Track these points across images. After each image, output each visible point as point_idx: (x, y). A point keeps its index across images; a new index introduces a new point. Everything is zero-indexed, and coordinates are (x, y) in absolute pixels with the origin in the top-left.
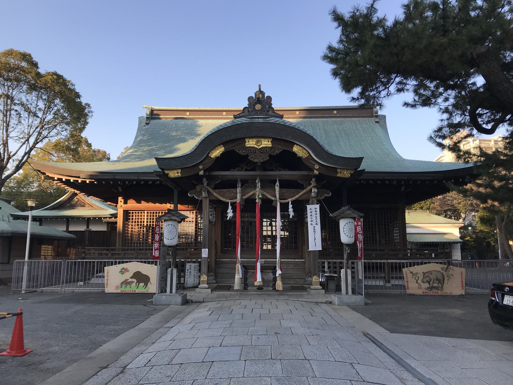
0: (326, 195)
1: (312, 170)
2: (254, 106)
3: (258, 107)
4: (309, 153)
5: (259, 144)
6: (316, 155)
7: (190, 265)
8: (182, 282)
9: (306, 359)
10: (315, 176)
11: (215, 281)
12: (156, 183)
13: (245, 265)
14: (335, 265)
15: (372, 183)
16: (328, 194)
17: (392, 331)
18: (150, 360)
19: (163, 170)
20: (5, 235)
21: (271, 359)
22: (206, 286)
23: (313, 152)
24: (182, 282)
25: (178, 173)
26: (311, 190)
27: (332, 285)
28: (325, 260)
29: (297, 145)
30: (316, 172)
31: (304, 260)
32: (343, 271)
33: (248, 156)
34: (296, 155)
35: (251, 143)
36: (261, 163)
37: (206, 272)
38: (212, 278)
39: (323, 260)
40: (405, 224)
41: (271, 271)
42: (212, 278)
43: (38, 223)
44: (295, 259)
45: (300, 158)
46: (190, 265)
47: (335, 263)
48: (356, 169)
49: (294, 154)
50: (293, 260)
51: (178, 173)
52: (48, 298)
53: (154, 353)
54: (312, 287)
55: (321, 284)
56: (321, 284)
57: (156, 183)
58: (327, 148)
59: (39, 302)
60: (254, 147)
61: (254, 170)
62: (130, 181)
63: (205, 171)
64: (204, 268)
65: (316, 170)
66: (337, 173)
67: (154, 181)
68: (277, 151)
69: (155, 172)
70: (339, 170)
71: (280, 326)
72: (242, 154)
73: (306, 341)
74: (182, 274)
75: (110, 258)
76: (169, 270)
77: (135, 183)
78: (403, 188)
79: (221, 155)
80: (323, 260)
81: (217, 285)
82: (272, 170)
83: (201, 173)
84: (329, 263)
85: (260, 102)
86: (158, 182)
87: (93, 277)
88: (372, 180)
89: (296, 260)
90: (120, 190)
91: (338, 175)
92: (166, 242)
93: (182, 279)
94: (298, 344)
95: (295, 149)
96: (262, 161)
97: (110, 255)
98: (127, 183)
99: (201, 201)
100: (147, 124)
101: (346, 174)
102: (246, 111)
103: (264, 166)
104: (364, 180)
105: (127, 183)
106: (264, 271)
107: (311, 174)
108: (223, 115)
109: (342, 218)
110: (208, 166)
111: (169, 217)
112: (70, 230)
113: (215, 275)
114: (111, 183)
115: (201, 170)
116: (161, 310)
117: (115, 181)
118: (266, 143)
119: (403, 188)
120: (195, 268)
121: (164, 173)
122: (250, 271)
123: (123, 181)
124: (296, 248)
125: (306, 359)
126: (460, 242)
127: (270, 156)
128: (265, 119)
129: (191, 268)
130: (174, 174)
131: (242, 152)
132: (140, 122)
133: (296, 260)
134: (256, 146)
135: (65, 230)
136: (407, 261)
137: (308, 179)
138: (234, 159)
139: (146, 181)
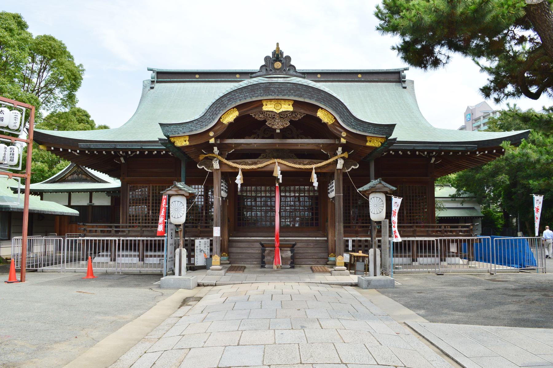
0: (353, 167)
1: (339, 139)
2: (273, 64)
3: (278, 65)
4: (335, 118)
5: (277, 108)
6: (343, 121)
7: (200, 242)
8: (192, 262)
9: (342, 363)
10: (342, 145)
11: (228, 262)
12: (162, 153)
13: (262, 242)
14: (360, 244)
15: (393, 153)
16: (356, 166)
17: (432, 321)
18: (154, 364)
19: (168, 137)
20: (3, 210)
21: (301, 363)
22: (220, 267)
23: (340, 117)
24: (192, 262)
25: (185, 141)
26: (337, 160)
27: (360, 266)
28: (349, 238)
29: (322, 108)
30: (343, 141)
31: (326, 239)
32: (371, 251)
33: (265, 121)
34: (321, 120)
35: (268, 107)
36: (281, 129)
37: (219, 250)
38: (225, 258)
39: (346, 239)
40: (434, 198)
41: (289, 249)
42: (225, 258)
43: (39, 197)
44: (316, 237)
45: (325, 124)
46: (200, 242)
47: (360, 241)
48: (387, 138)
49: (319, 120)
50: (314, 238)
51: (185, 141)
52: (47, 280)
53: (159, 354)
54: (337, 268)
55: (346, 265)
56: (346, 265)
57: (162, 153)
58: (354, 114)
59: (38, 284)
60: (272, 112)
61: (271, 137)
62: (133, 151)
63: (216, 139)
64: (217, 247)
65: (344, 138)
66: (367, 141)
67: (159, 151)
68: (299, 116)
69: (160, 139)
70: (368, 139)
71: (306, 317)
72: (259, 119)
73: (339, 337)
74: (192, 254)
75: (113, 236)
76: (178, 250)
77: (138, 152)
78: (433, 159)
79: (235, 120)
80: (346, 239)
81: (230, 265)
82: (293, 138)
83: (212, 141)
84: (353, 241)
85: (278, 61)
86: (164, 152)
87: (95, 256)
88: (402, 150)
89: (317, 239)
90: (123, 161)
91: (368, 144)
92: (172, 220)
93: (192, 259)
94: (330, 341)
95: (320, 114)
96: (282, 127)
97: (113, 232)
98: (130, 153)
99: (211, 174)
100: (152, 88)
101: (374, 143)
102: (264, 71)
103: (285, 133)
104: (393, 150)
105: (130, 153)
106: (283, 249)
107: (337, 142)
108: (237, 78)
109: (372, 192)
110: (219, 133)
111: (176, 191)
112: (72, 204)
113: (228, 256)
114: (112, 152)
115: (211, 137)
116: (169, 295)
117: (117, 150)
118: (288, 107)
119: (433, 159)
120: (205, 244)
121: (170, 141)
122: (267, 249)
123: (125, 151)
124: (317, 224)
125: (342, 363)
126: (481, 217)
127: (291, 121)
128: (285, 79)
129: (201, 244)
130: (181, 142)
131: (260, 117)
132: (145, 87)
133: (317, 239)
134: (275, 110)
135: (67, 204)
136: (437, 238)
137: (333, 150)
138: (250, 122)
139: (151, 151)
